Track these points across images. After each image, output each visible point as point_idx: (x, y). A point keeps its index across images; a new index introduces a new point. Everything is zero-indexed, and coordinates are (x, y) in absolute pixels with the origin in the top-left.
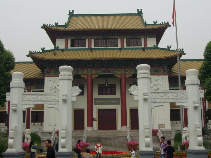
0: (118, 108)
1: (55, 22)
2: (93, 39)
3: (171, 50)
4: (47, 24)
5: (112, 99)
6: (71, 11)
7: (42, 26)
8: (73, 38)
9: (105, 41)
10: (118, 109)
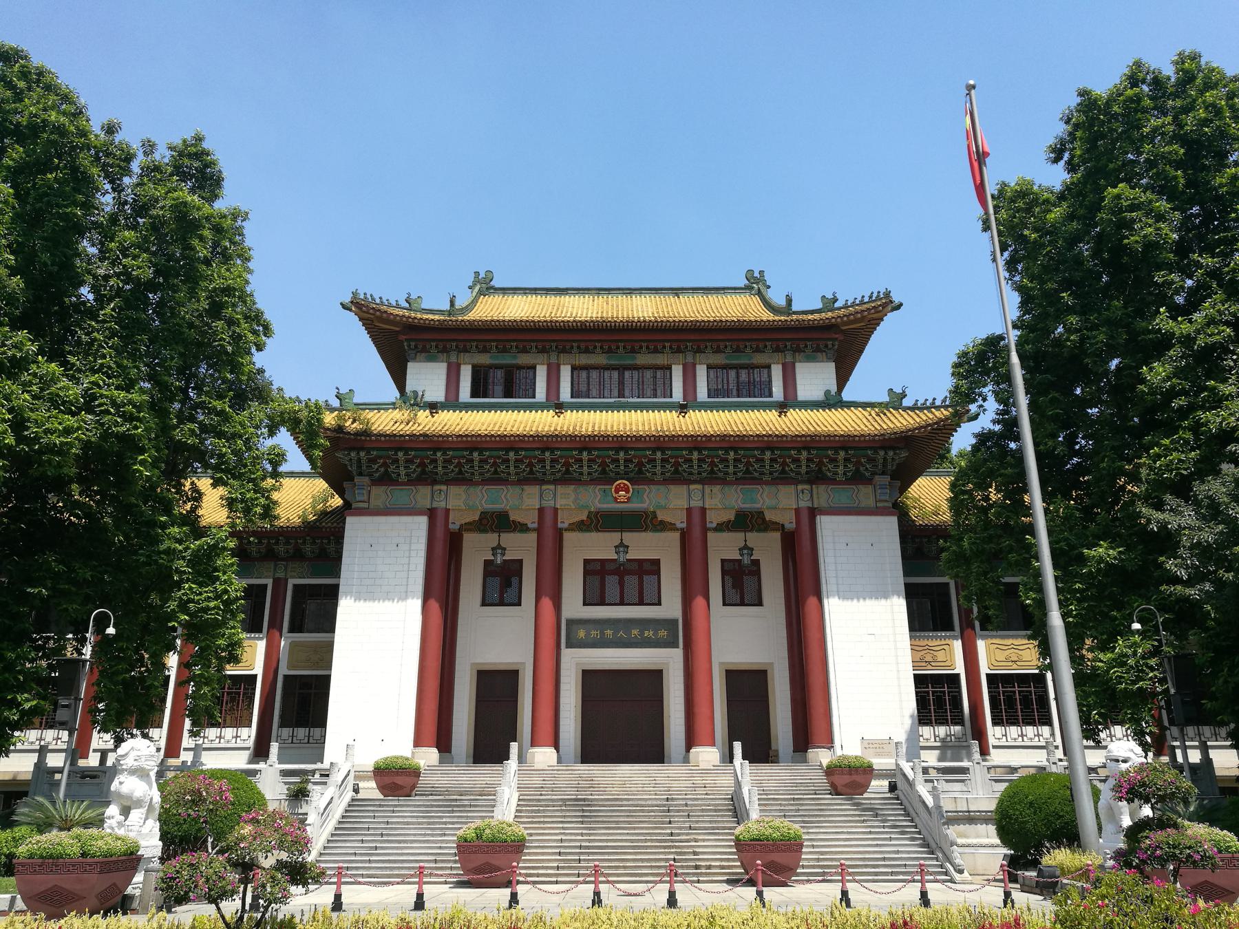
0: (671, 660)
1: (409, 294)
2: (569, 367)
3: (909, 408)
4: (369, 296)
5: (644, 623)
6: (482, 275)
7: (347, 299)
8: (484, 359)
9: (615, 374)
10: (671, 671)
